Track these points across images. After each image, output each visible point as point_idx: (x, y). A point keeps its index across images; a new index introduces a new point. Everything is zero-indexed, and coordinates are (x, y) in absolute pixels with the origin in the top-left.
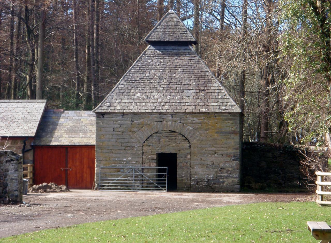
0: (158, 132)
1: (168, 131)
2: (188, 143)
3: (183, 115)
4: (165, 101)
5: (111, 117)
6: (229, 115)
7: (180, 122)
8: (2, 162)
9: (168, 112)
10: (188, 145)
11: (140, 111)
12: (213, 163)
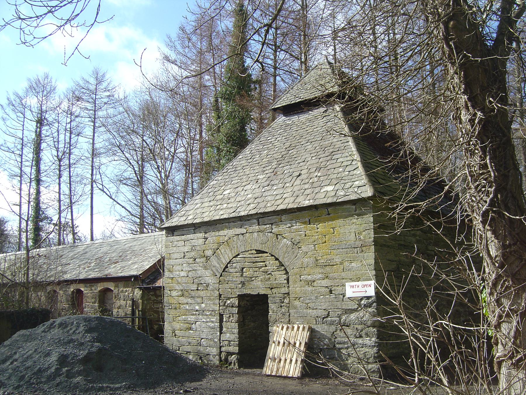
0: (239, 255)
1: (254, 252)
2: (284, 272)
3: (275, 216)
4: (345, 164)
5: (182, 233)
6: (354, 207)
7: (271, 232)
8: (62, 355)
9: (251, 215)
10: (285, 277)
11: (266, 211)
12: (327, 313)
